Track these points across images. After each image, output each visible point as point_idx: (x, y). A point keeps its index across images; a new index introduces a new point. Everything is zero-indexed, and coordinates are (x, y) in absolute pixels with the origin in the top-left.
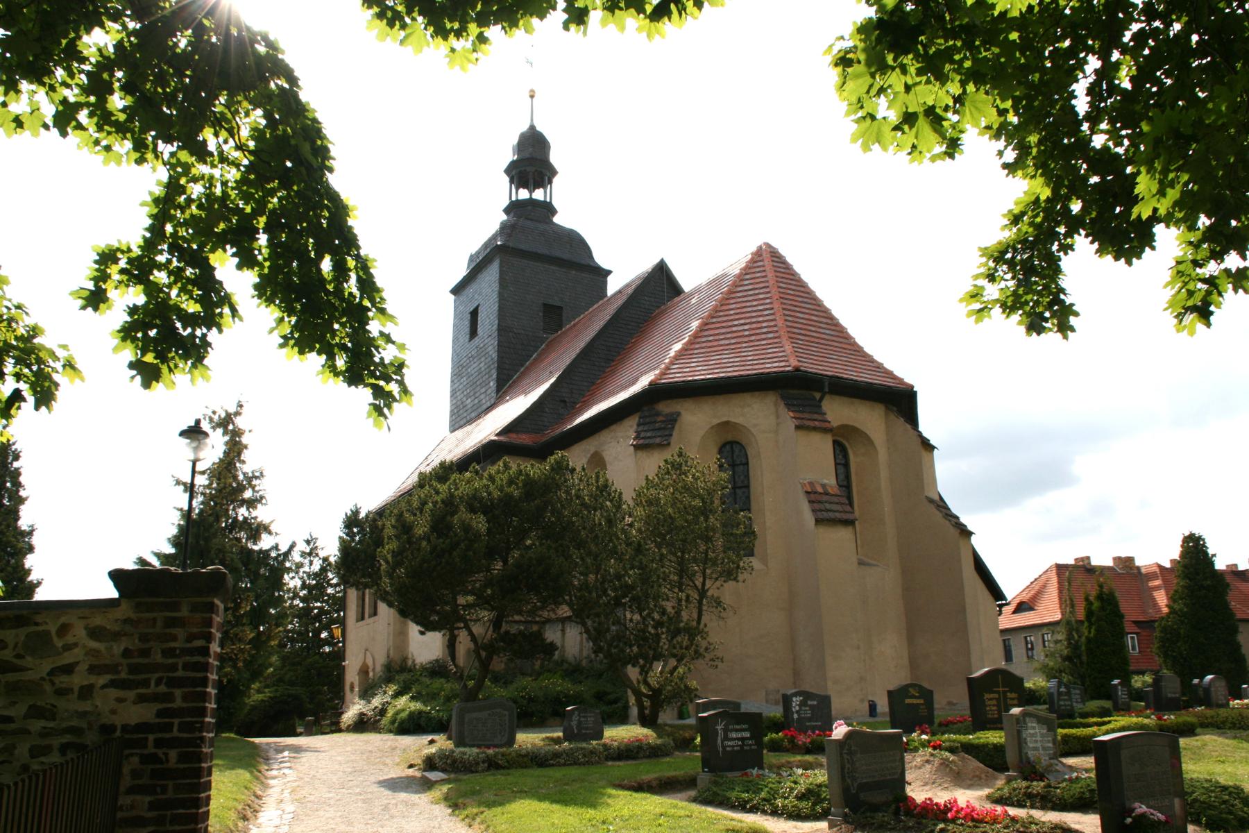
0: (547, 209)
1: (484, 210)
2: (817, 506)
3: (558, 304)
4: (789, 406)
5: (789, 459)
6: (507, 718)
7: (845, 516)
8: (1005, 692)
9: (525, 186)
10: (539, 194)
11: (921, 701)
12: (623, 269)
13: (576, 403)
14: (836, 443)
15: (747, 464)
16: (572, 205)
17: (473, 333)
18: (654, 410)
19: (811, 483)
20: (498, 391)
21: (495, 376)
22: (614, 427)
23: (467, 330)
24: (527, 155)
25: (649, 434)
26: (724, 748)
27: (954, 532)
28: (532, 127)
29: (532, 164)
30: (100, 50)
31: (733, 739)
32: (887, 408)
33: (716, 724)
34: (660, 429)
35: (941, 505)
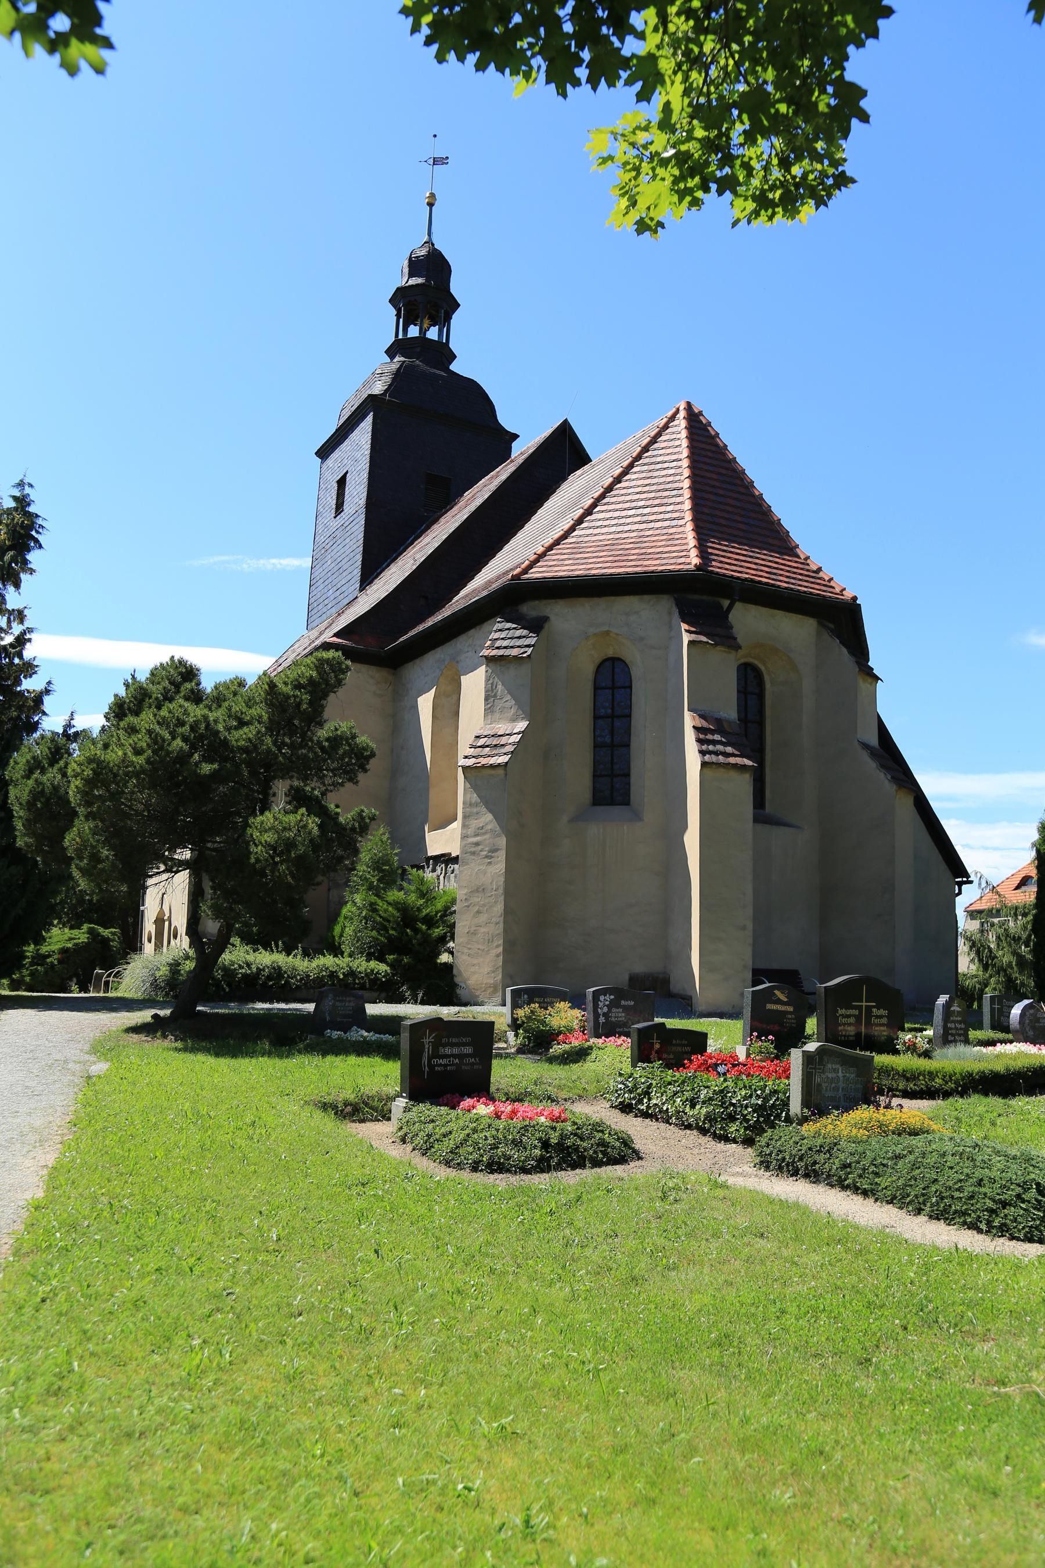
0: (443, 353)
1: (362, 358)
8: (869, 1009)
11: (790, 1009)
16: (475, 350)
22: (472, 632)
29: (427, 292)
31: (446, 1056)
32: (820, 623)
35: (887, 753)
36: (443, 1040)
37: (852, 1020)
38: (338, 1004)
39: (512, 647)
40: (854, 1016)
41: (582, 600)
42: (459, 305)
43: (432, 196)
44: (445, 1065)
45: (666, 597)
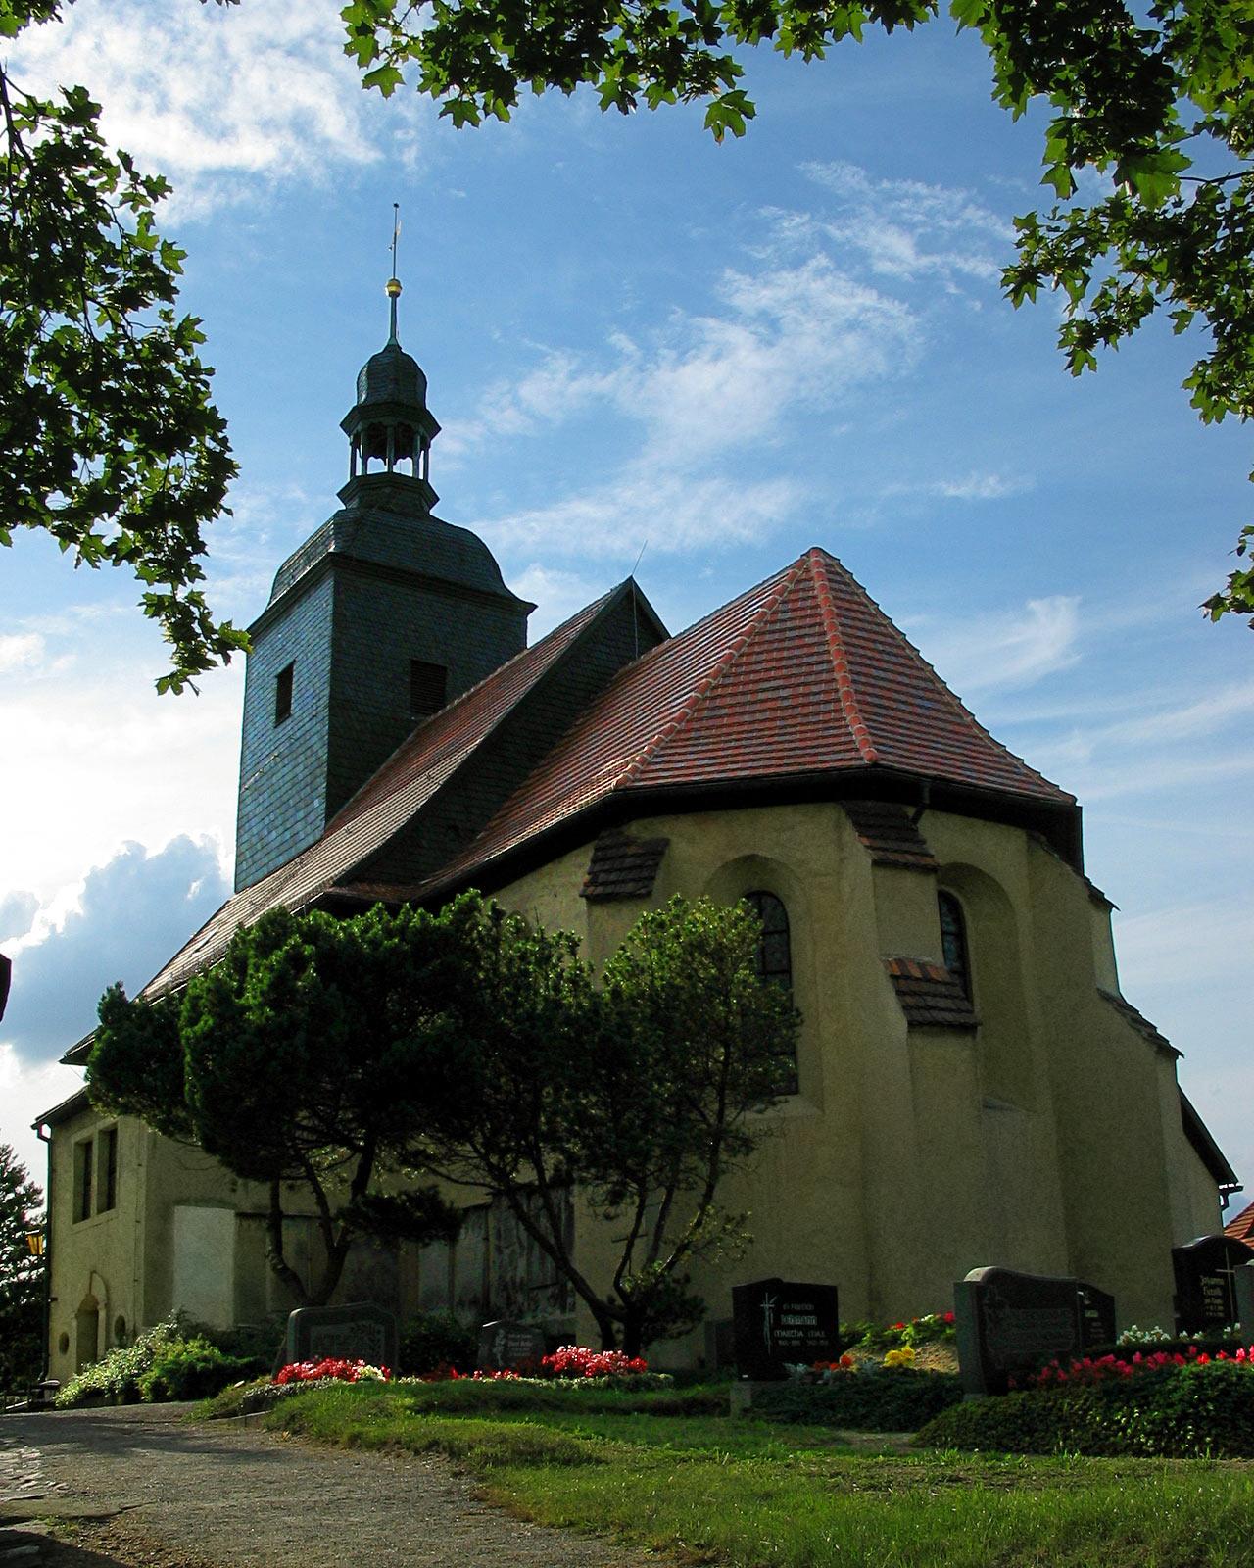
0: (421, 493)
2: (909, 999)
3: (440, 662)
4: (863, 828)
5: (857, 922)
6: (382, 1336)
7: (962, 1019)
9: (379, 453)
10: (404, 467)
12: (553, 602)
13: (475, 832)
14: (944, 897)
15: (786, 931)
17: (283, 711)
18: (618, 841)
19: (900, 962)
20: (330, 812)
21: (322, 789)
23: (272, 707)
24: (384, 396)
25: (613, 877)
26: (775, 1339)
27: (1147, 1051)
28: (393, 348)
30: (121, 21)
31: (791, 1327)
32: (1031, 837)
33: (762, 1300)
34: (630, 869)
36: (784, 1307)
37: (1218, 1291)
38: (511, 1343)
39: (623, 882)
40: (1221, 1287)
41: (715, 814)
42: (440, 429)
43: (395, 282)
44: (789, 1339)
45: (832, 804)
